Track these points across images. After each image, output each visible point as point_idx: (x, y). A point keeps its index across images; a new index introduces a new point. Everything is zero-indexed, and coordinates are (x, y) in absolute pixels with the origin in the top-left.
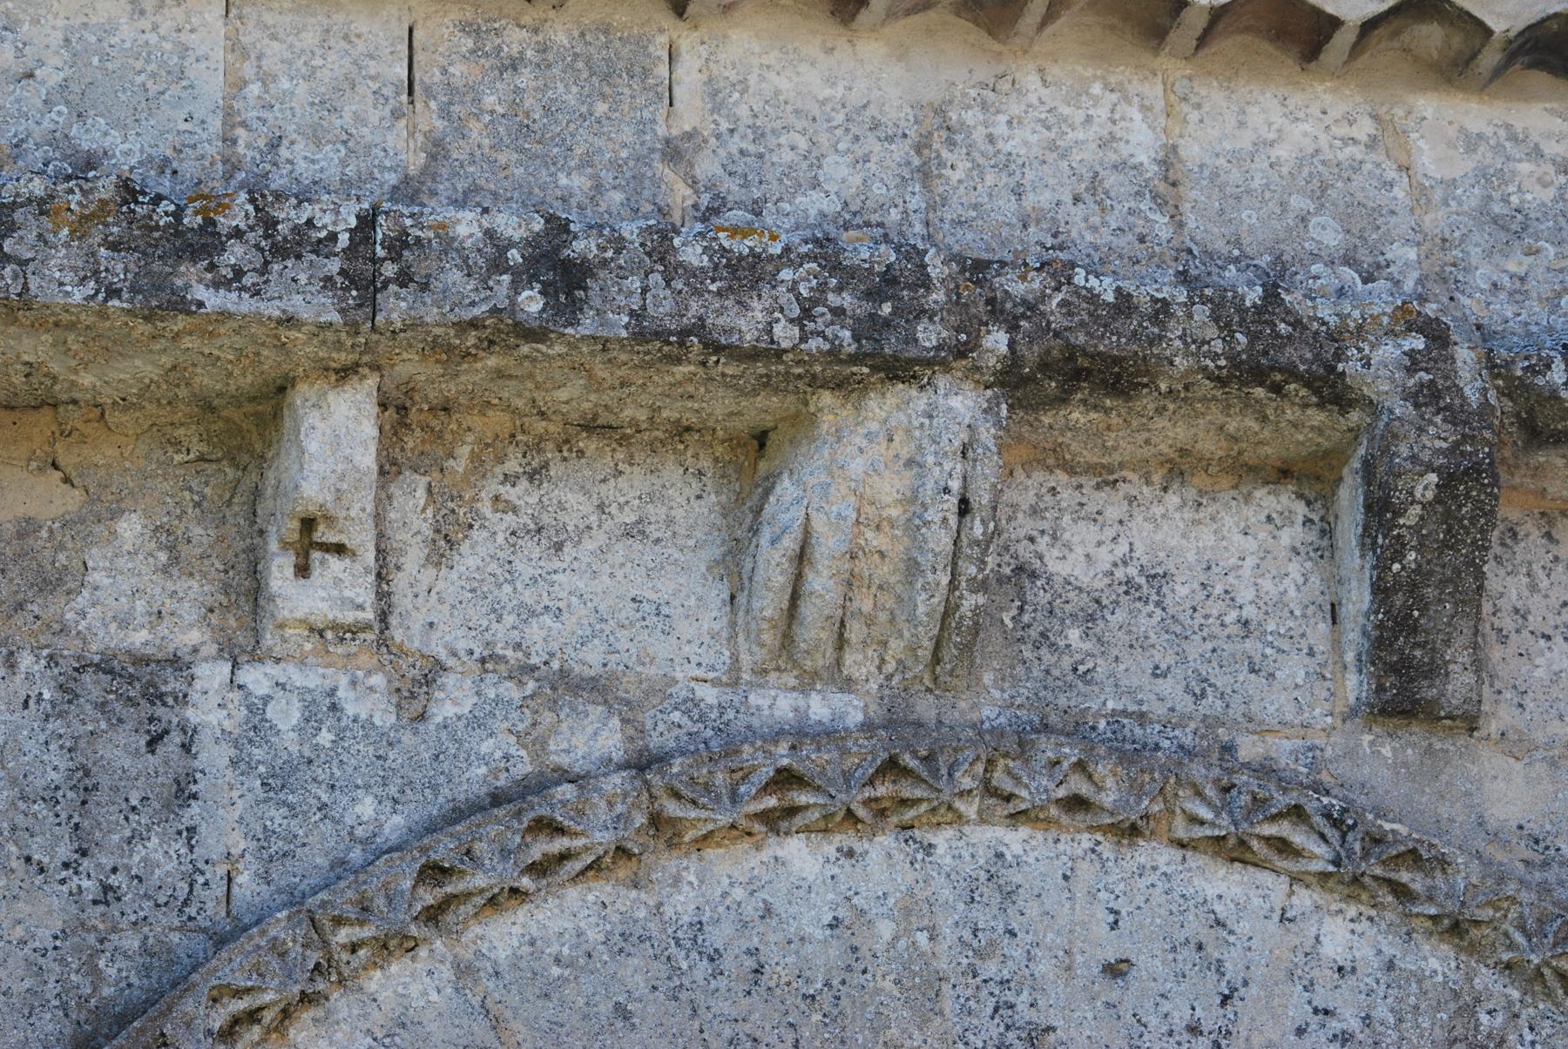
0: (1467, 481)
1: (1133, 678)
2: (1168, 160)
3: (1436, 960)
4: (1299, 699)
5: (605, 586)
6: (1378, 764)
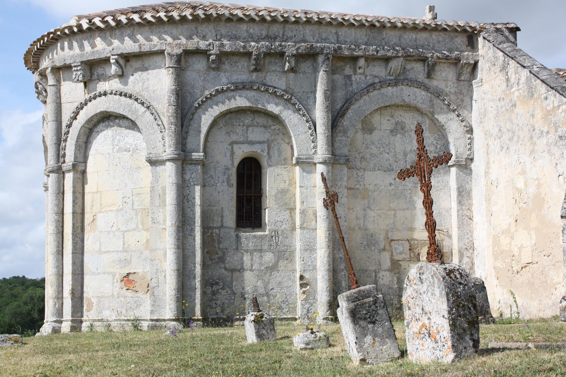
0: (434, 65)
1: (411, 75)
2: (416, 38)
3: (429, 95)
4: (421, 77)
5: (379, 71)
6: (426, 81)
